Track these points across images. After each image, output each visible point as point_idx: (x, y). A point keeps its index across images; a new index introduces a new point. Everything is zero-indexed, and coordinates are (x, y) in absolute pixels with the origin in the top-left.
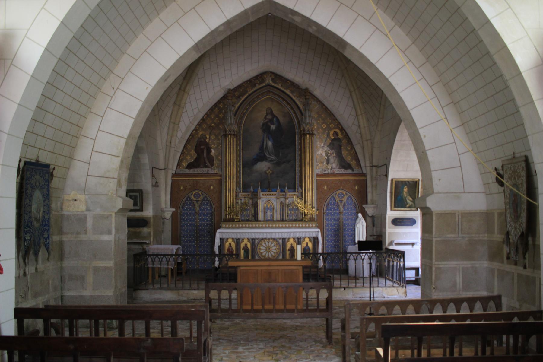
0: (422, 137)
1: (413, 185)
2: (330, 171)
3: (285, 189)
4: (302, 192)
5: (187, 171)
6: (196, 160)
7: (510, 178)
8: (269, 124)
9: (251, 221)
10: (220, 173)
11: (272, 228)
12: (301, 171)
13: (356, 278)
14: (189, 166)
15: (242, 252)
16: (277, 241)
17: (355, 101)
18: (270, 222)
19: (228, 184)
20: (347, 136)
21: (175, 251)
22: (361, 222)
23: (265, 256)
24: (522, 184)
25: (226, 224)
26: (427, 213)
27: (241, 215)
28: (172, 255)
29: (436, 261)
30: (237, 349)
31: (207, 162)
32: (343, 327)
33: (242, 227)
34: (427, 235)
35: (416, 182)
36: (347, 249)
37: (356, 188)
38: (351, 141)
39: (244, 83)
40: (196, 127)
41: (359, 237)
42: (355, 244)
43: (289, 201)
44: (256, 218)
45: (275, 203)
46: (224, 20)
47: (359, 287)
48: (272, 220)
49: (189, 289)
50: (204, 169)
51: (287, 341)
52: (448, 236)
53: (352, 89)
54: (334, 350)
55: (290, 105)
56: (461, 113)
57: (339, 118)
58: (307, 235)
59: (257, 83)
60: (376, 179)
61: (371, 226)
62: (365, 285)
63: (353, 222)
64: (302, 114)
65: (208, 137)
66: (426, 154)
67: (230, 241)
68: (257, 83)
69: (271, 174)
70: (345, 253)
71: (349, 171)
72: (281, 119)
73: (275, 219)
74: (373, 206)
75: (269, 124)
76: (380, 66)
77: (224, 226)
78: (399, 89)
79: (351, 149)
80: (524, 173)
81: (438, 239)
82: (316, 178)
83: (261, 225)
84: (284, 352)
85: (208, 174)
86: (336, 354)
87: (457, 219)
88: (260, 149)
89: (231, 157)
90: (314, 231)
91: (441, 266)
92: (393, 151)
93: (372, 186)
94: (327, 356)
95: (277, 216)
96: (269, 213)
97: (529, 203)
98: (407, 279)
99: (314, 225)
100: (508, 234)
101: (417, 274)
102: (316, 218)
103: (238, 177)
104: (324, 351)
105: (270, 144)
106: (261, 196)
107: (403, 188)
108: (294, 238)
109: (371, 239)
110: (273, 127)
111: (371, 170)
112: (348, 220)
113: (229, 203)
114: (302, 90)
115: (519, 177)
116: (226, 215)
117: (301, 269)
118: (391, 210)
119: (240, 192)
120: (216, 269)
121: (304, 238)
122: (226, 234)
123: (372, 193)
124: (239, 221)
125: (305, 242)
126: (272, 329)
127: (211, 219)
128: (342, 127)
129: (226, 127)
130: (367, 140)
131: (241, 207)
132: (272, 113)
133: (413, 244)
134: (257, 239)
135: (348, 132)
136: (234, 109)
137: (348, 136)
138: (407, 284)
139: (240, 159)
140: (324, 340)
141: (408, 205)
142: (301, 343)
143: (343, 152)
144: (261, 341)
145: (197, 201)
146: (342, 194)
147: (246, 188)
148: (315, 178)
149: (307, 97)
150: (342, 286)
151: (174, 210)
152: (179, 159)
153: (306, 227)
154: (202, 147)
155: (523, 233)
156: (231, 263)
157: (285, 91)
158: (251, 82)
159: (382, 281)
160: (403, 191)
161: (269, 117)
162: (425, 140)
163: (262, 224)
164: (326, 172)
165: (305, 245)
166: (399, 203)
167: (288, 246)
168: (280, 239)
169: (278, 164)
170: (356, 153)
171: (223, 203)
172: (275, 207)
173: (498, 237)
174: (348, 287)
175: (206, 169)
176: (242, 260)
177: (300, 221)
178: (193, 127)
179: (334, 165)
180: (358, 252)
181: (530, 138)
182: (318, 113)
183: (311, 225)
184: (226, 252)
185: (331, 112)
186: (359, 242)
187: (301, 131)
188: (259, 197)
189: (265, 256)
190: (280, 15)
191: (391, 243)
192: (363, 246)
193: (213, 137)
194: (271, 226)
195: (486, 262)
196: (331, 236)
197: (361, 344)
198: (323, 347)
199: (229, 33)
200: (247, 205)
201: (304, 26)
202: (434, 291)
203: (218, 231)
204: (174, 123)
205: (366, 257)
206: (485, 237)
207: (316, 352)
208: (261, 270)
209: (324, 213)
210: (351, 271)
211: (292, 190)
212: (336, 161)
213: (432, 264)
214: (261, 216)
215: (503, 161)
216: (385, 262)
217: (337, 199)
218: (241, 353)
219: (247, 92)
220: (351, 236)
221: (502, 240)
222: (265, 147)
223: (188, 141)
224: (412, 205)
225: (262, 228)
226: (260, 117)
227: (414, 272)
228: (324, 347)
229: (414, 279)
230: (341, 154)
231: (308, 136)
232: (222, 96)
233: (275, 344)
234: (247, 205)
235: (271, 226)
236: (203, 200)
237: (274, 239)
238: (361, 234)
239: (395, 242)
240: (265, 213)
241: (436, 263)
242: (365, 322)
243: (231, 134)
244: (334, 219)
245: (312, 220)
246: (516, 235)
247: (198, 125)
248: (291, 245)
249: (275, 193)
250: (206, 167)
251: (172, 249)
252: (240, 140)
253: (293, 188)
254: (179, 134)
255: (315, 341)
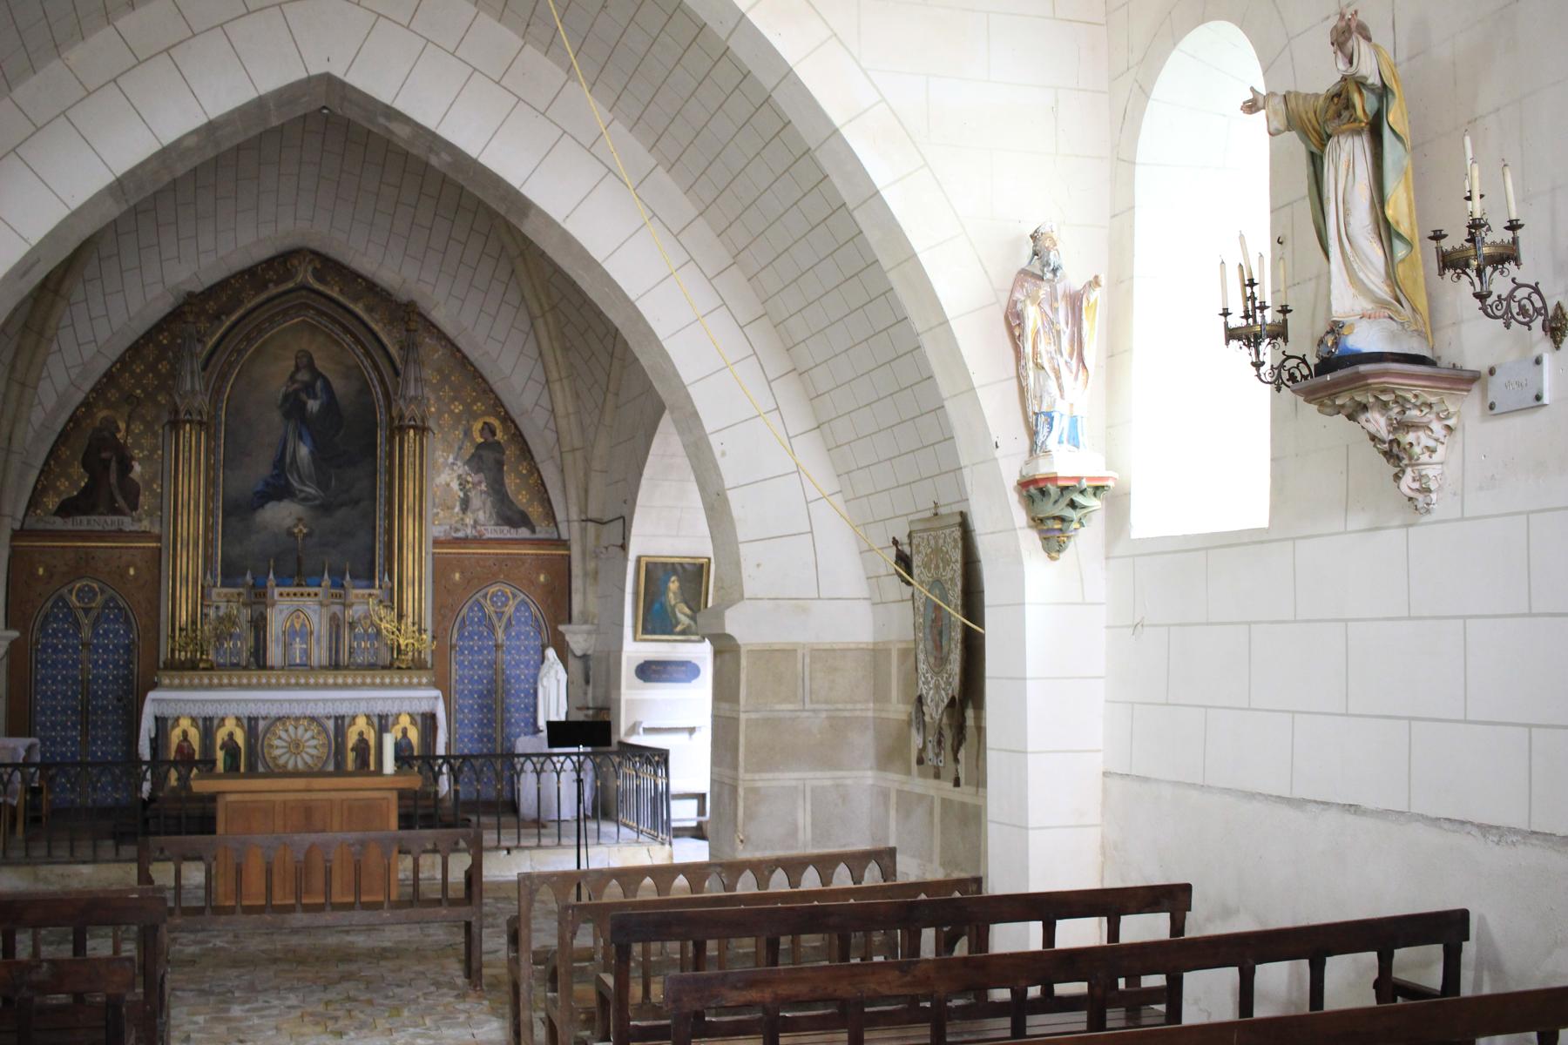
0: (717, 454)
1: (694, 575)
2: (470, 532)
3: (343, 578)
4: (392, 589)
5: (59, 523)
6: (84, 492)
7: (926, 566)
8: (303, 396)
9: (246, 668)
10: (156, 530)
11: (307, 686)
12: (389, 531)
13: (539, 823)
14: (66, 509)
15: (220, 755)
16: (320, 724)
17: (545, 343)
18: (298, 671)
19: (182, 561)
20: (518, 437)
21: (23, 753)
22: (552, 673)
23: (285, 766)
24: (952, 579)
25: (172, 678)
26: (725, 649)
27: (217, 650)
28: (15, 766)
29: (746, 771)
30: (228, 1010)
31: (119, 498)
32: (514, 939)
33: (221, 686)
34: (725, 706)
35: (702, 565)
36: (513, 746)
37: (542, 578)
38: (529, 451)
39: (234, 276)
40: (87, 398)
41: (547, 712)
42: (537, 731)
43: (356, 611)
44: (258, 660)
45: (315, 619)
46: (201, 121)
47: (547, 847)
48: (306, 667)
49: (70, 863)
50: (109, 519)
51: (362, 986)
52: (778, 707)
53: (536, 311)
54: (486, 1002)
55: (363, 346)
56: (814, 397)
57: (499, 387)
58: (406, 707)
59: (271, 281)
60: (597, 556)
61: (581, 681)
62: (564, 841)
63: (532, 671)
64: (397, 373)
65: (122, 425)
66: (726, 501)
67: (185, 723)
68: (271, 281)
69: (306, 536)
70: (510, 756)
71: (523, 533)
72: (338, 385)
73: (315, 661)
74: (585, 627)
75: (303, 396)
76: (615, 269)
77: (167, 681)
78: (661, 332)
79: (531, 473)
80: (957, 555)
81: (753, 716)
82: (431, 550)
83: (273, 681)
84: (355, 1013)
85: (119, 534)
86: (494, 1012)
87: (800, 666)
88: (275, 467)
89: (190, 486)
90: (428, 698)
91: (760, 784)
92: (644, 481)
93: (586, 574)
94: (470, 1017)
95: (320, 655)
96: (298, 645)
97: (966, 629)
98: (674, 824)
99: (424, 680)
100: (920, 700)
101: (701, 811)
102: (429, 659)
103: (209, 543)
104: (461, 1006)
105: (304, 451)
106: (276, 597)
107: (667, 582)
108: (368, 717)
109: (579, 716)
110: (313, 405)
111: (584, 531)
112: (517, 665)
113: (183, 617)
114: (399, 305)
115: (947, 563)
116: (173, 651)
117: (393, 796)
118: (635, 639)
119: (215, 585)
120: (146, 804)
121: (398, 716)
122: (177, 706)
123: (585, 593)
124: (211, 668)
125: (398, 728)
126: (317, 959)
127: (128, 663)
128: (506, 412)
129: (178, 400)
130: (574, 450)
131: (216, 629)
132: (311, 366)
133: (692, 730)
134: (265, 718)
135: (522, 427)
136: (203, 351)
137: (521, 435)
138: (676, 836)
139: (216, 493)
140: (461, 981)
141: (679, 628)
142: (398, 991)
143: (507, 481)
144: (291, 989)
145: (87, 611)
146: (504, 594)
147: (231, 574)
148: (428, 549)
149: (413, 326)
150: (503, 843)
151: (15, 634)
152: (35, 488)
153: (401, 686)
154: (104, 455)
155: (953, 700)
156: (200, 786)
157: (351, 306)
158: (254, 276)
159: (608, 828)
160: (667, 588)
161: (304, 376)
162: (724, 465)
163: (278, 677)
164: (460, 534)
165: (400, 735)
166: (656, 621)
167: (352, 739)
168: (328, 718)
169: (325, 508)
170: (543, 484)
171: (163, 618)
172: (316, 628)
173: (898, 710)
174: (518, 847)
175: (115, 518)
176: (220, 776)
177: (384, 668)
178: (79, 397)
179: (481, 516)
180: (547, 750)
181: (966, 472)
182: (440, 371)
183: (415, 680)
184: (172, 756)
185: (476, 370)
186: (550, 724)
187: (392, 418)
188: (269, 601)
189: (285, 766)
190: (353, 113)
191: (633, 730)
192: (560, 734)
193: (137, 427)
194: (302, 681)
195: (870, 773)
196: (471, 710)
197: (561, 971)
198: (457, 996)
199: (210, 153)
200: (234, 624)
201: (418, 151)
202: (741, 847)
203: (151, 695)
204: (23, 385)
205: (568, 765)
206: (867, 710)
207: (440, 1009)
208: (285, 802)
209: (452, 647)
210: (527, 804)
211: (365, 583)
212: (489, 504)
213: (736, 779)
214: (274, 654)
215: (911, 522)
216: (618, 777)
217: (489, 609)
218: (240, 1020)
219: (241, 302)
220: (526, 708)
221: (904, 717)
222: (288, 460)
223: (63, 437)
224: (689, 626)
225: (278, 687)
226: (277, 375)
227: (694, 803)
228: (462, 996)
229: (694, 824)
230: (502, 484)
231: (412, 432)
232: (168, 309)
233: (331, 995)
234: (234, 624)
235: (302, 681)
236: (106, 606)
237: (313, 719)
238: (554, 702)
239: (646, 725)
240: (287, 646)
241: (748, 776)
242: (570, 917)
243: (191, 422)
244: (480, 664)
245: (418, 665)
246: (937, 706)
247: (92, 390)
248: (361, 734)
249: (316, 590)
250: (117, 512)
251: (15, 749)
252: (216, 438)
253: (366, 575)
254: (37, 416)
255: (438, 984)
